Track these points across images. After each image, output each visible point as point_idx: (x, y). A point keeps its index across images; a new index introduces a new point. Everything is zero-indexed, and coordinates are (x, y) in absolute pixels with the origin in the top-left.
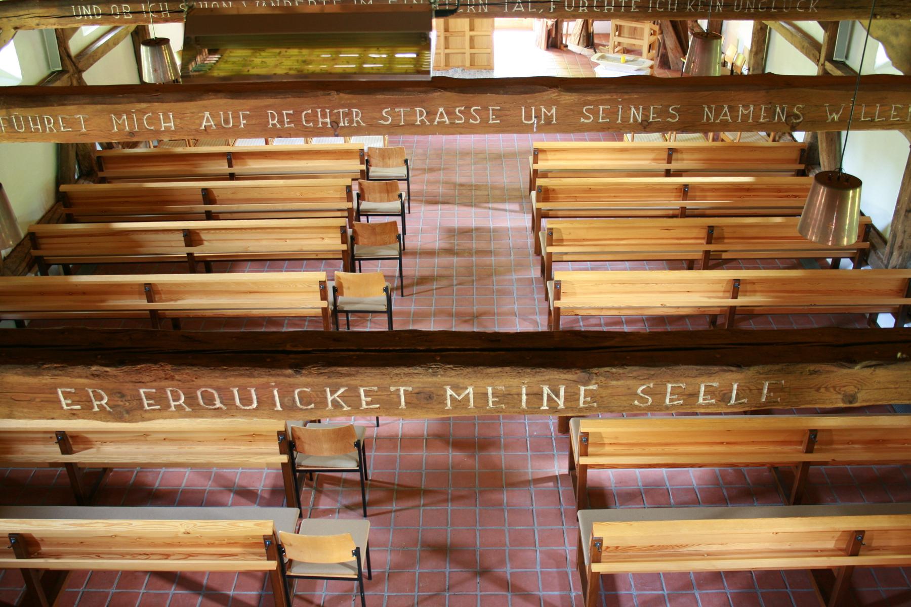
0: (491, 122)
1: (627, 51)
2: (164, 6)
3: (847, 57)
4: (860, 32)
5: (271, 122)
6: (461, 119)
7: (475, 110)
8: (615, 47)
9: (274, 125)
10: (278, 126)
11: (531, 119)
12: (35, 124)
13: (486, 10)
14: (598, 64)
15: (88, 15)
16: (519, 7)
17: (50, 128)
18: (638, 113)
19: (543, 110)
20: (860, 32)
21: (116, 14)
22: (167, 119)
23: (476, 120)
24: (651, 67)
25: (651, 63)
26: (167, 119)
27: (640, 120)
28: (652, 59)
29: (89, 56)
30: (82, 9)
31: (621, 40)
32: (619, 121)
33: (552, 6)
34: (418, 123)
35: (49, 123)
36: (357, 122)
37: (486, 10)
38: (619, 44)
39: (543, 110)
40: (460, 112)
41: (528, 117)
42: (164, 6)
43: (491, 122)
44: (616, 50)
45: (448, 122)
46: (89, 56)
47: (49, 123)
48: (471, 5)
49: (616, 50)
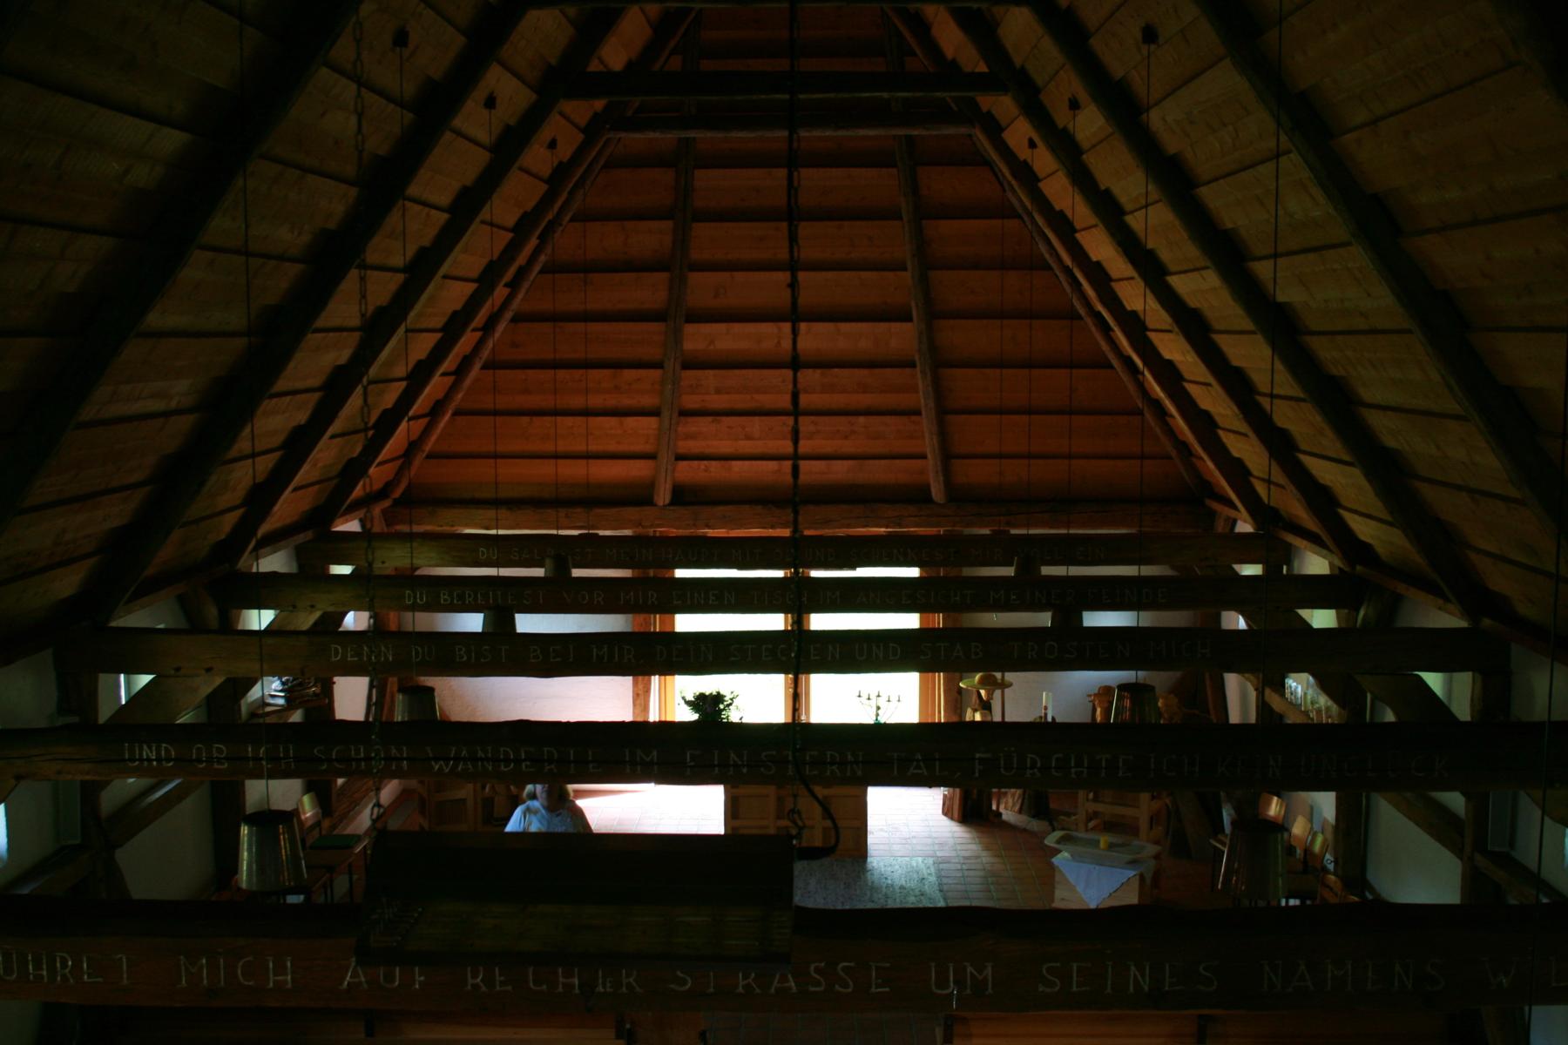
0: (873, 990)
1: (1110, 826)
2: (286, 751)
3: (1512, 845)
4: (1530, 812)
5: (470, 981)
6: (818, 984)
7: (844, 969)
8: (1090, 819)
9: (476, 987)
10: (484, 989)
11: (947, 987)
12: (38, 967)
13: (859, 773)
14: (1059, 851)
15: (149, 760)
16: (918, 767)
17: (64, 976)
18: (1143, 976)
19: (969, 969)
20: (1530, 812)
21: (200, 761)
22: (279, 969)
23: (846, 986)
24: (1157, 857)
25: (1158, 848)
26: (279, 969)
27: (1146, 988)
28: (1157, 843)
29: (133, 818)
30: (141, 750)
31: (1100, 807)
32: (1109, 990)
33: (978, 767)
34: (740, 989)
35: (64, 965)
36: (629, 985)
37: (859, 773)
38: (1096, 814)
39: (969, 969)
40: (817, 970)
41: (942, 983)
42: (286, 751)
43: (873, 990)
44: (1091, 825)
45: (794, 989)
46: (133, 818)
47: (64, 965)
48: (832, 763)
49: (1091, 825)
